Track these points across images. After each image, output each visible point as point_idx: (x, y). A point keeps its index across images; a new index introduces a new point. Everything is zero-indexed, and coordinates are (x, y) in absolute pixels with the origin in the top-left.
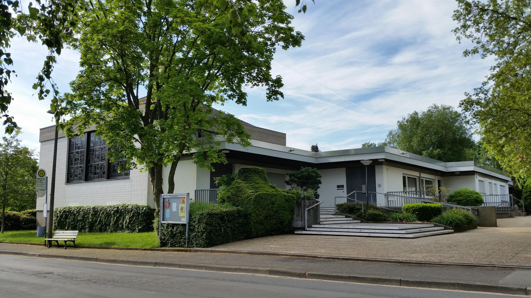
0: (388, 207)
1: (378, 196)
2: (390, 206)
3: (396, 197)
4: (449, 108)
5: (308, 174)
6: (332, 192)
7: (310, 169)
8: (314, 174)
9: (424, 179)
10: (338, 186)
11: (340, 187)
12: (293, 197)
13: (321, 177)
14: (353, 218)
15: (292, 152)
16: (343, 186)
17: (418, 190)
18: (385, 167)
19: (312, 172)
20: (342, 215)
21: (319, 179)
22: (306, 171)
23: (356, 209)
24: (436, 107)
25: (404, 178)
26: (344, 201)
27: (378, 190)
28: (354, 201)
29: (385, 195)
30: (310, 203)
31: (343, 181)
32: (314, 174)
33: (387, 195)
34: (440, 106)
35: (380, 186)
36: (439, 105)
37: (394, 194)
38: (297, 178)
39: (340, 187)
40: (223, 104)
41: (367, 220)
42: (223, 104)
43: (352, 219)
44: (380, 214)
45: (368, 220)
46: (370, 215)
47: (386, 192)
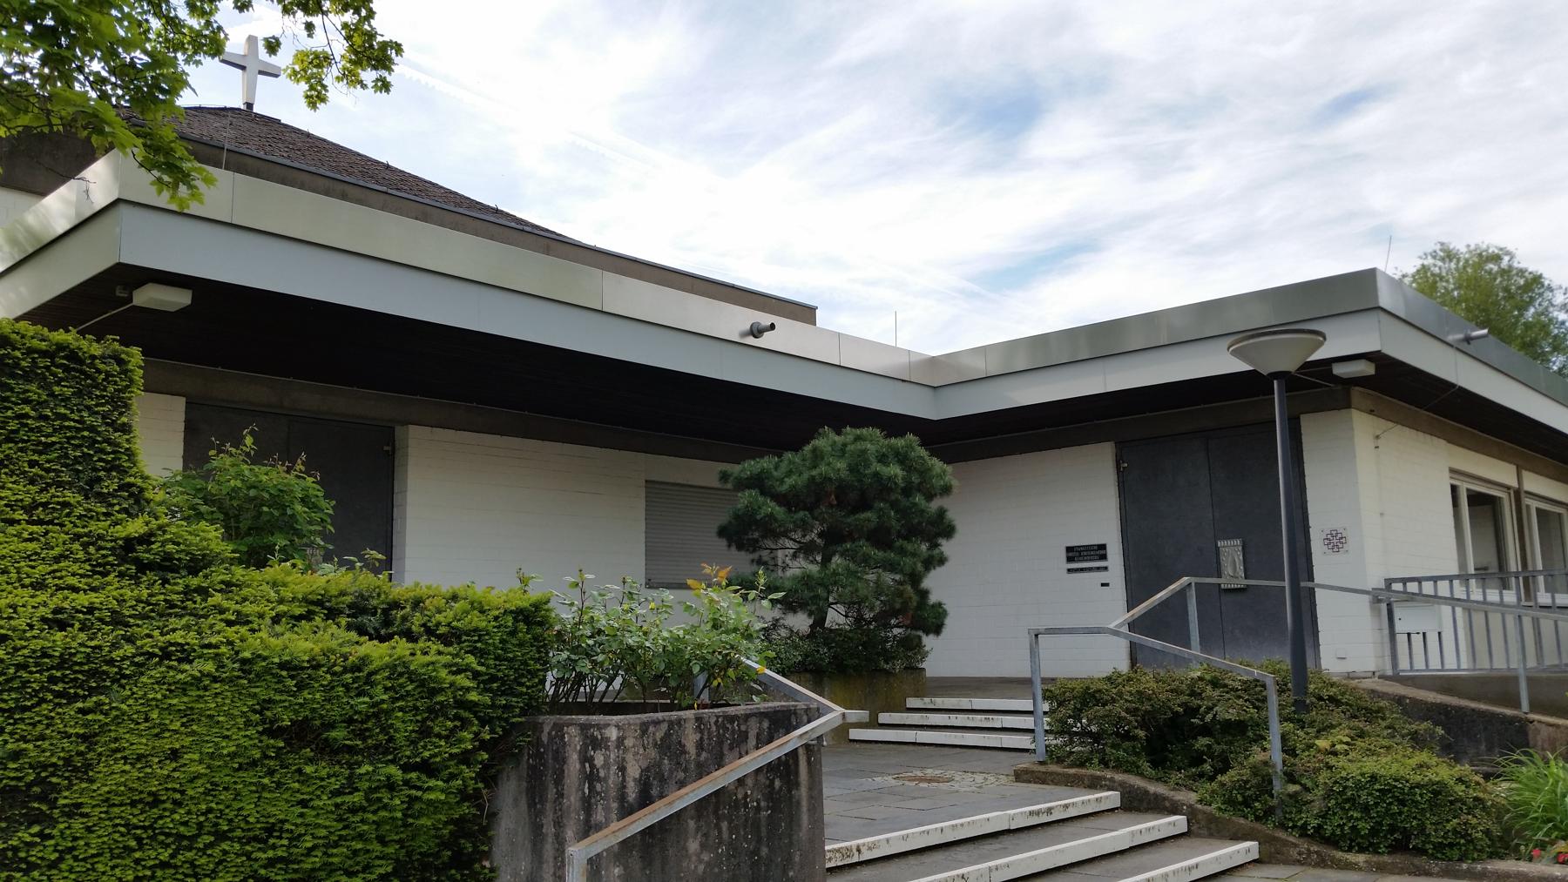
0: (1397, 678)
1: (1325, 603)
2: (1404, 664)
3: (1446, 610)
4: (1496, 258)
5: (853, 469)
6: (1033, 592)
7: (873, 440)
8: (895, 470)
9: (1534, 504)
10: (1074, 554)
11: (1083, 555)
12: (428, 687)
13: (946, 490)
14: (1192, 816)
15: (762, 342)
16: (1099, 552)
17: (1514, 564)
18: (1362, 426)
19: (882, 459)
20: (1094, 784)
21: (934, 505)
22: (842, 451)
23: (1206, 730)
24: (1449, 255)
25: (1454, 489)
26: (1102, 657)
27: (1325, 567)
28: (1183, 662)
29: (1377, 600)
30: (670, 746)
31: (1100, 519)
32: (895, 470)
33: (1388, 600)
34: (1463, 249)
35: (1336, 541)
36: (1460, 246)
37: (1428, 588)
38: (780, 499)
39: (1083, 555)
40: (384, 86)
41: (1318, 835)
42: (384, 86)
43: (1178, 822)
44: (1438, 791)
45: (1333, 842)
46: (1344, 797)
47: (1375, 580)
